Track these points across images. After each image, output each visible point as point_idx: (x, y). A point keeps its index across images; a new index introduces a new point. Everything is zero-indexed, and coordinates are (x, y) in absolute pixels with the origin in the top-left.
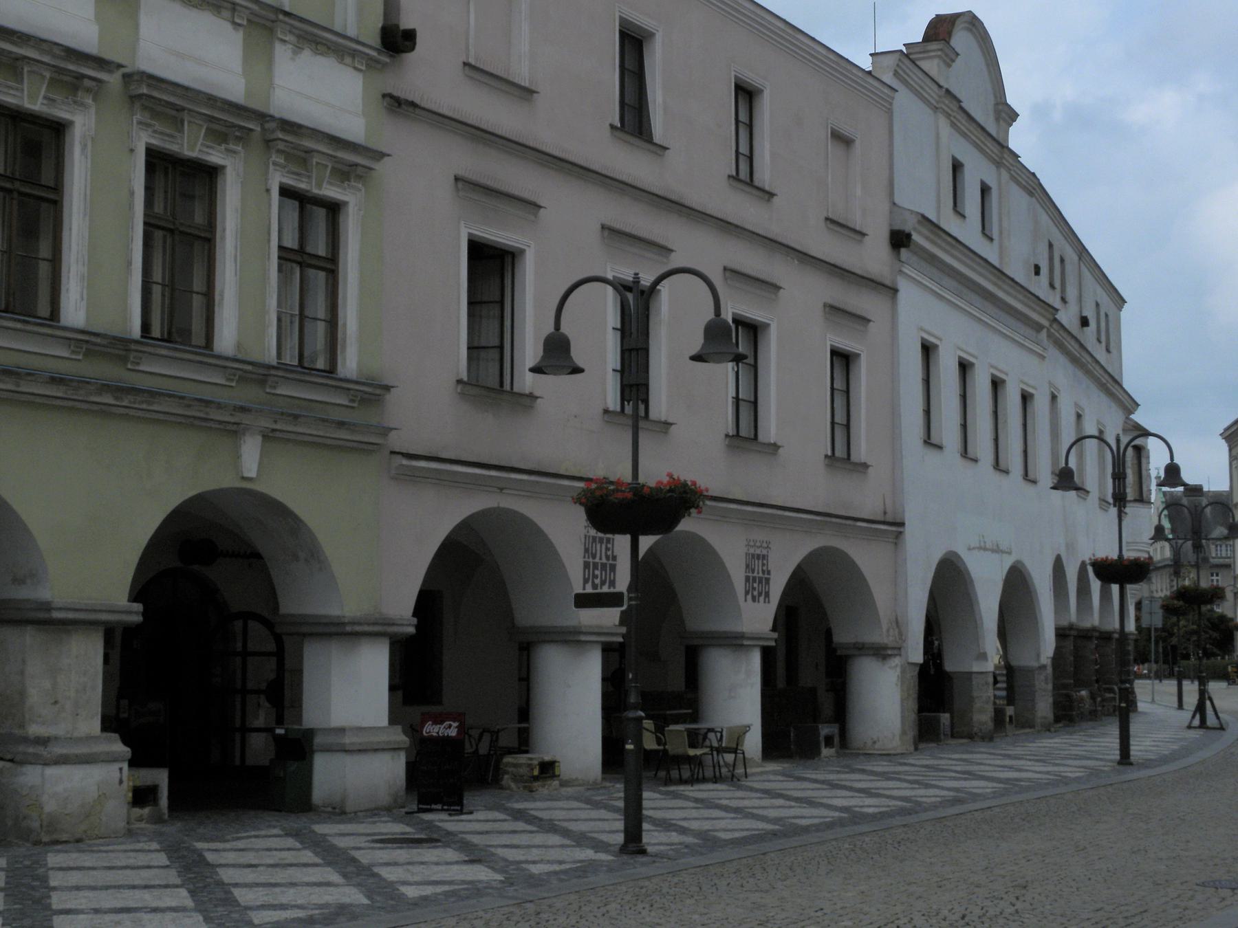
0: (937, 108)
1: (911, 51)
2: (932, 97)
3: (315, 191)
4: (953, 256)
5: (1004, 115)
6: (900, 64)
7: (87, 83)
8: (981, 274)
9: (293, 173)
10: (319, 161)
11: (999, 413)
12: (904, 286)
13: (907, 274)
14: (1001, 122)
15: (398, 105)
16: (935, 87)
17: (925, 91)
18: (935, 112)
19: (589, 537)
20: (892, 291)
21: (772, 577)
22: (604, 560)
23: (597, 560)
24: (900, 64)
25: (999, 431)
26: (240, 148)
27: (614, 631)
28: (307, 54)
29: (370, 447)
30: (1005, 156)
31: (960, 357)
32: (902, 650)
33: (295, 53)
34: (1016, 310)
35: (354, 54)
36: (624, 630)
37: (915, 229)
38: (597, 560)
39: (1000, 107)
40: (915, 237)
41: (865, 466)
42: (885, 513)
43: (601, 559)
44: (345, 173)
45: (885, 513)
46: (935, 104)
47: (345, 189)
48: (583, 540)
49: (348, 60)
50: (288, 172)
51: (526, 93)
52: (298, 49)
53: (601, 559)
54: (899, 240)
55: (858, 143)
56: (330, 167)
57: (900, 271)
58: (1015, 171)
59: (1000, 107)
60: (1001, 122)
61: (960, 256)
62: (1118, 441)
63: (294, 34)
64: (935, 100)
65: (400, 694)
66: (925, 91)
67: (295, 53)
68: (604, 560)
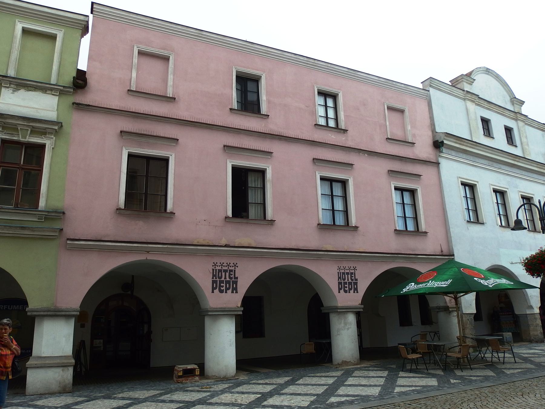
0: (465, 99)
1: (452, 83)
2: (519, 117)
3: (22, 139)
4: (478, 149)
5: (515, 102)
6: (431, 82)
7: (48, 131)
8: (502, 157)
9: (8, 134)
10: (21, 128)
11: (533, 210)
12: (441, 160)
13: (443, 156)
14: (515, 105)
15: (79, 106)
16: (461, 91)
17: (454, 92)
18: (465, 101)
19: (340, 273)
20: (438, 164)
21: (359, 282)
22: (350, 281)
23: (346, 281)
24: (431, 82)
25: (534, 217)
26: (53, 136)
27: (238, 309)
28: (22, 92)
29: (54, 237)
30: (518, 116)
31: (521, 195)
32: (460, 308)
33: (14, 91)
34: (536, 171)
35: (51, 90)
36: (362, 306)
37: (444, 139)
38: (346, 281)
39: (513, 100)
40: (445, 142)
41: (426, 233)
42: (442, 251)
43: (348, 280)
44: (43, 133)
45: (442, 251)
46: (463, 97)
47: (43, 138)
48: (211, 271)
49: (49, 92)
50: (5, 133)
51: (172, 99)
52: (16, 90)
53: (348, 280)
54: (438, 145)
55: (171, 58)
56: (30, 130)
57: (440, 156)
58: (477, 101)
59: (513, 100)
60: (515, 105)
61: (540, 167)
62: (540, 202)
63: (13, 84)
64: (464, 96)
65: (241, 334)
66: (454, 92)
67: (14, 91)
68: (350, 281)
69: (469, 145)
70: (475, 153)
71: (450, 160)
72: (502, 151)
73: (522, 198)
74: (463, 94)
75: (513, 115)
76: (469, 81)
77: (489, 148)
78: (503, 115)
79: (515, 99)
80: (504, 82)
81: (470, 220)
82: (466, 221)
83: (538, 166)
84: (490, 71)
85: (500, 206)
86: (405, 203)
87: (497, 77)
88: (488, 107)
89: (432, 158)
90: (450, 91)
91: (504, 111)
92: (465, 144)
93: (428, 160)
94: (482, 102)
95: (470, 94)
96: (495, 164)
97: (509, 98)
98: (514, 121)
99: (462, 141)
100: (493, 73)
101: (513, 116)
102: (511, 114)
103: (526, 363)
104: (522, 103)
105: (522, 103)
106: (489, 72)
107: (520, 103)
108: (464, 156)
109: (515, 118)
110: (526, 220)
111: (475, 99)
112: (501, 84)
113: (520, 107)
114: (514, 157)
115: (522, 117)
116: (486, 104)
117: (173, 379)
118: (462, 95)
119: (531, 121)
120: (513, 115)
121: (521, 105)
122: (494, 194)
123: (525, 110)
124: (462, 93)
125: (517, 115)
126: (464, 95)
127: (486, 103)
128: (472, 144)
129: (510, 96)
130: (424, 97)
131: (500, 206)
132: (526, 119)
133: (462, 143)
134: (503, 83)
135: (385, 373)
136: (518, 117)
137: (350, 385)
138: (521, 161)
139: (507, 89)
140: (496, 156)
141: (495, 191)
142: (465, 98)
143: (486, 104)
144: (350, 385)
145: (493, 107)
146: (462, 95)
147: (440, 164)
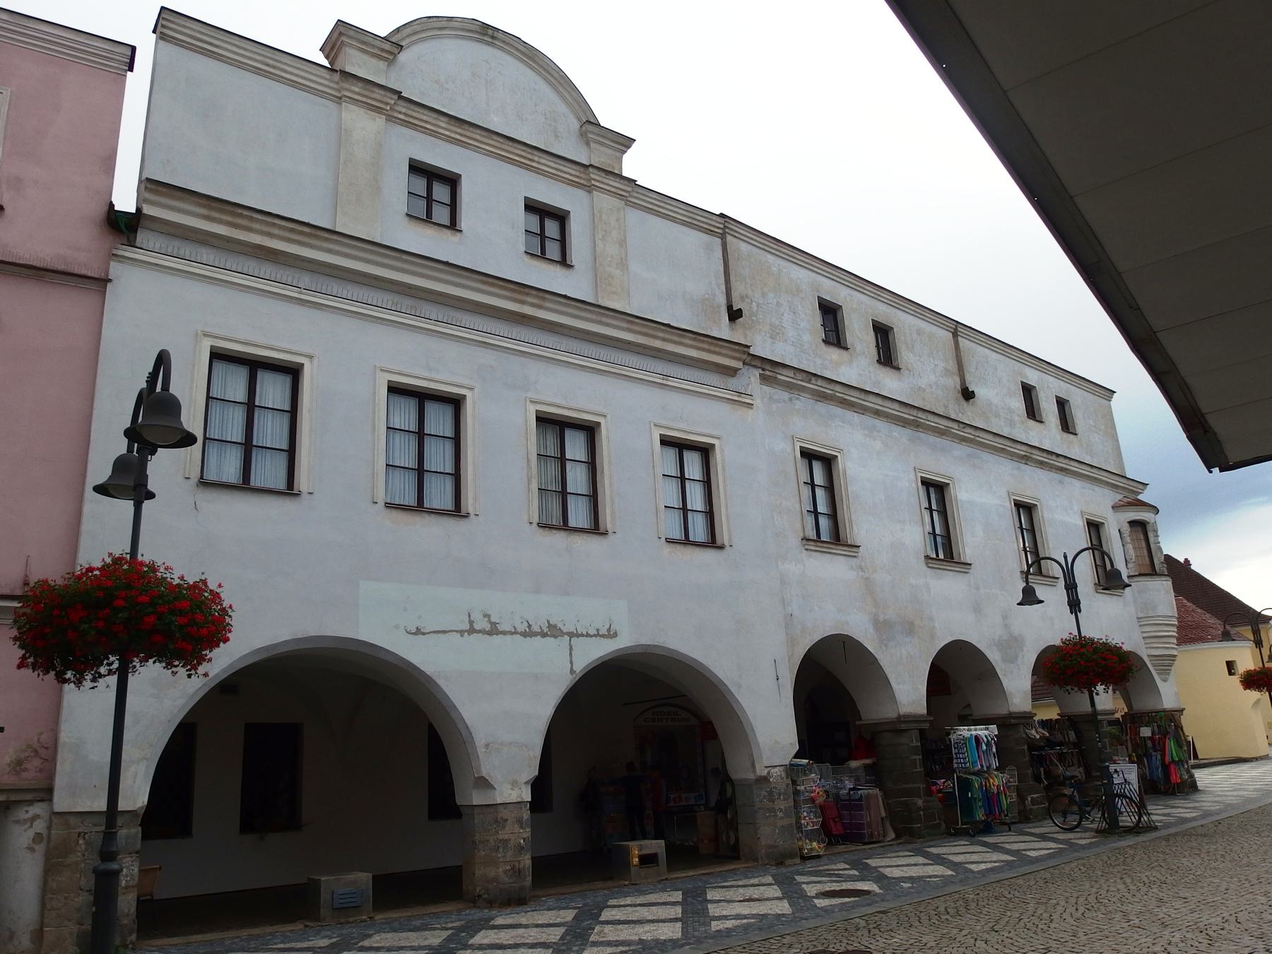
0: (340, 98)
4: (330, 251)
8: (457, 285)
12: (115, 269)
34: (629, 343)
69: (276, 231)
70: (546, 323)
71: (448, 339)
72: (447, 263)
73: (1015, 505)
74: (331, 81)
75: (578, 174)
76: (373, 46)
77: (388, 252)
78: (527, 169)
79: (591, 128)
80: (556, 75)
81: (937, 555)
82: (535, 525)
83: (636, 328)
84: (500, 35)
85: (935, 515)
86: (689, 508)
87: (530, 58)
88: (458, 137)
89: (86, 262)
90: (268, 65)
91: (879, 293)
92: (325, 245)
93: (61, 267)
94: (425, 118)
95: (360, 85)
96: (187, 249)
97: (575, 125)
98: (581, 193)
99: (241, 216)
100: (512, 42)
101: (577, 177)
102: (566, 169)
103: (1018, 851)
104: (626, 142)
105: (626, 142)
106: (493, 37)
107: (613, 141)
108: (268, 269)
109: (582, 181)
110: (1023, 552)
111: (387, 104)
112: (545, 79)
113: (618, 154)
114: (513, 291)
115: (612, 183)
116: (443, 125)
117: (77, 946)
118: (326, 82)
119: (659, 201)
120: (578, 174)
121: (624, 149)
122: (923, 488)
123: (631, 166)
124: (328, 76)
125: (588, 174)
126: (335, 86)
127: (443, 123)
128: (292, 230)
129: (579, 120)
130: (111, 66)
131: (935, 515)
132: (629, 189)
133: (239, 221)
134: (555, 79)
135: (678, 896)
136: (594, 179)
137: (608, 922)
138: (548, 305)
139: (571, 96)
140: (339, 258)
141: (926, 483)
142: (339, 95)
143: (443, 125)
144: (608, 922)
145: (478, 137)
146: (326, 82)
147: (109, 286)
